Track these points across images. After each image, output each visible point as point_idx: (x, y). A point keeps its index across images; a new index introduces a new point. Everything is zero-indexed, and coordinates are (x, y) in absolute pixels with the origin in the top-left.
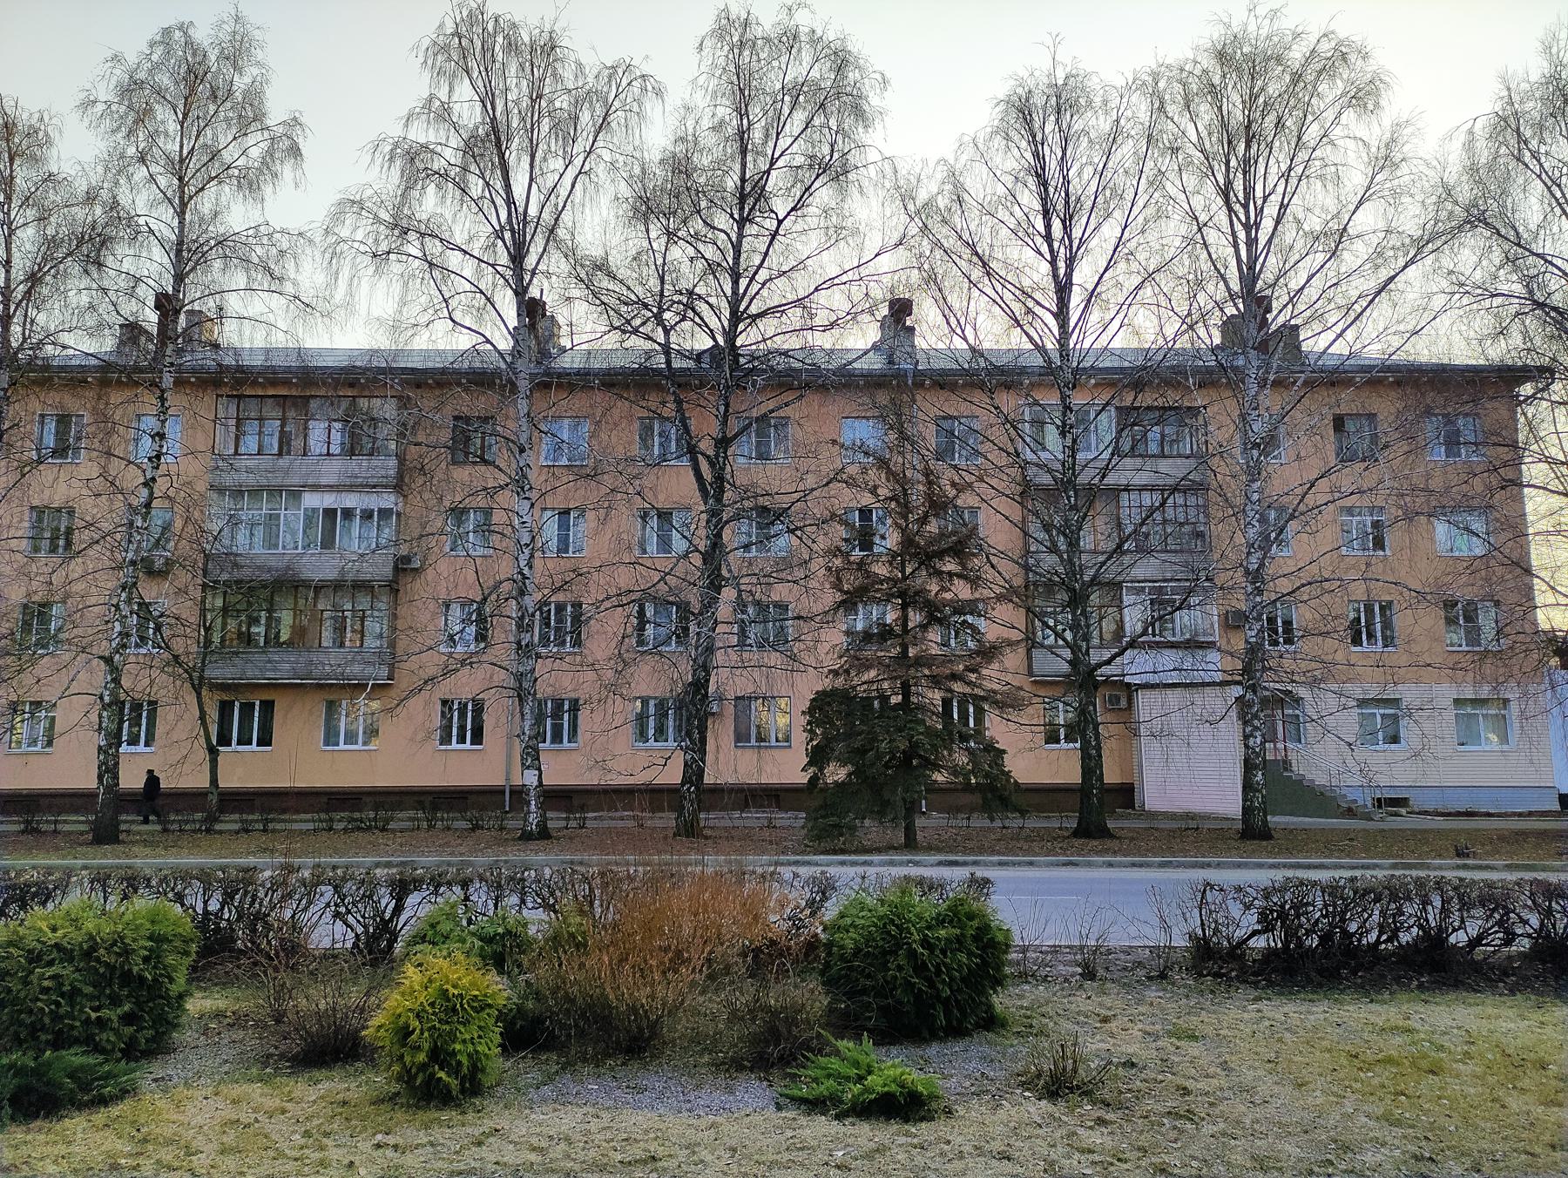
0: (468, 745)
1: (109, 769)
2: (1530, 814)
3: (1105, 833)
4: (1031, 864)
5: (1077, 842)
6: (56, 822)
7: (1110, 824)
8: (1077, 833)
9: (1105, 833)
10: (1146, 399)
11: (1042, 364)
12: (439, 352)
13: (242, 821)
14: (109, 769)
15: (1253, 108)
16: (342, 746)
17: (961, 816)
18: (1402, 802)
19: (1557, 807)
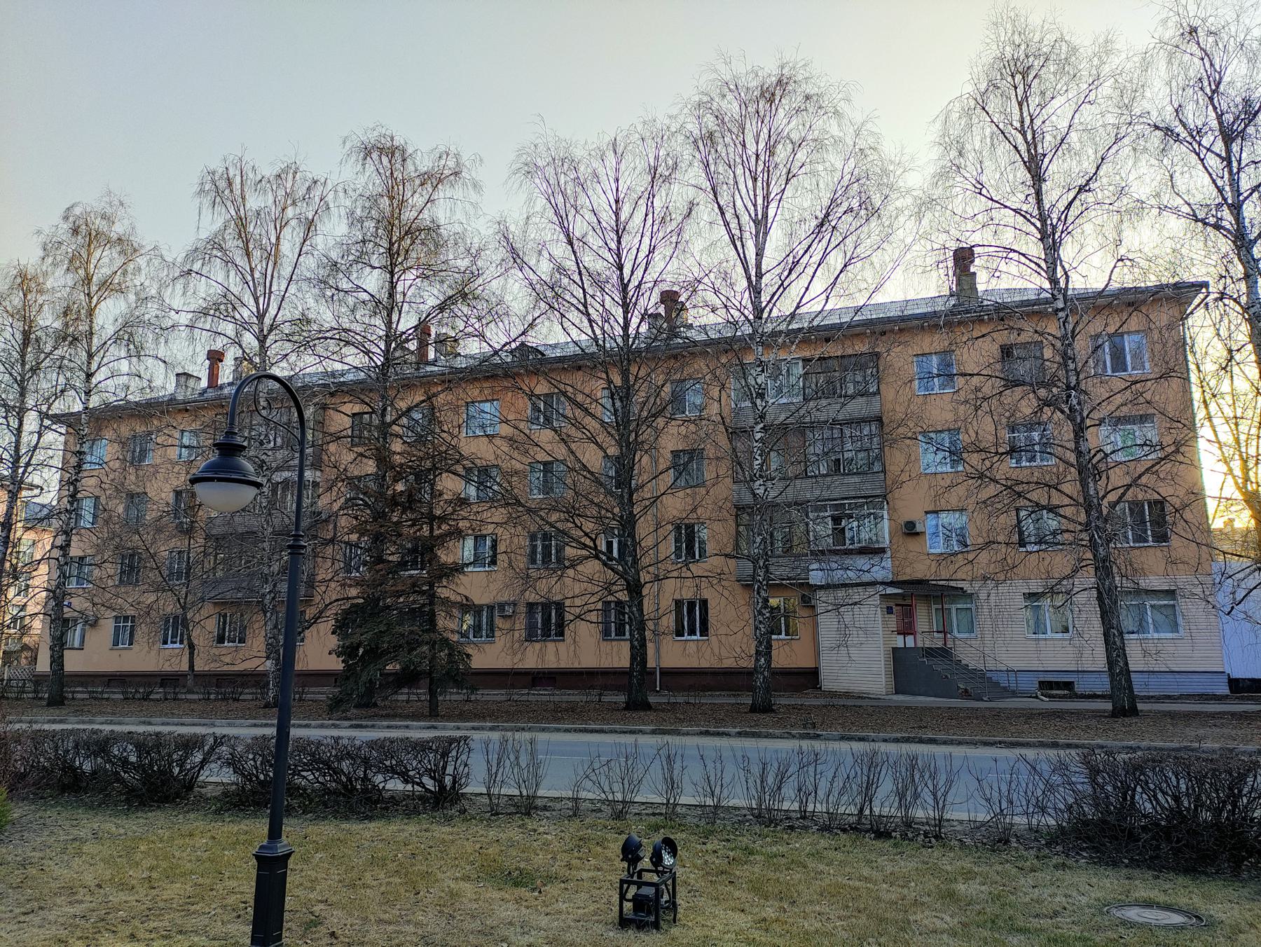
0: (783, 636)
1: (765, 650)
2: (1181, 697)
3: (647, 707)
4: (373, 726)
5: (755, 716)
6: (73, 692)
7: (652, 699)
8: (754, 709)
9: (647, 707)
10: (833, 350)
11: (219, 382)
12: (916, 302)
13: (89, 692)
14: (765, 650)
15: (750, 132)
16: (1049, 635)
17: (595, 692)
18: (1068, 685)
19: (1226, 691)
